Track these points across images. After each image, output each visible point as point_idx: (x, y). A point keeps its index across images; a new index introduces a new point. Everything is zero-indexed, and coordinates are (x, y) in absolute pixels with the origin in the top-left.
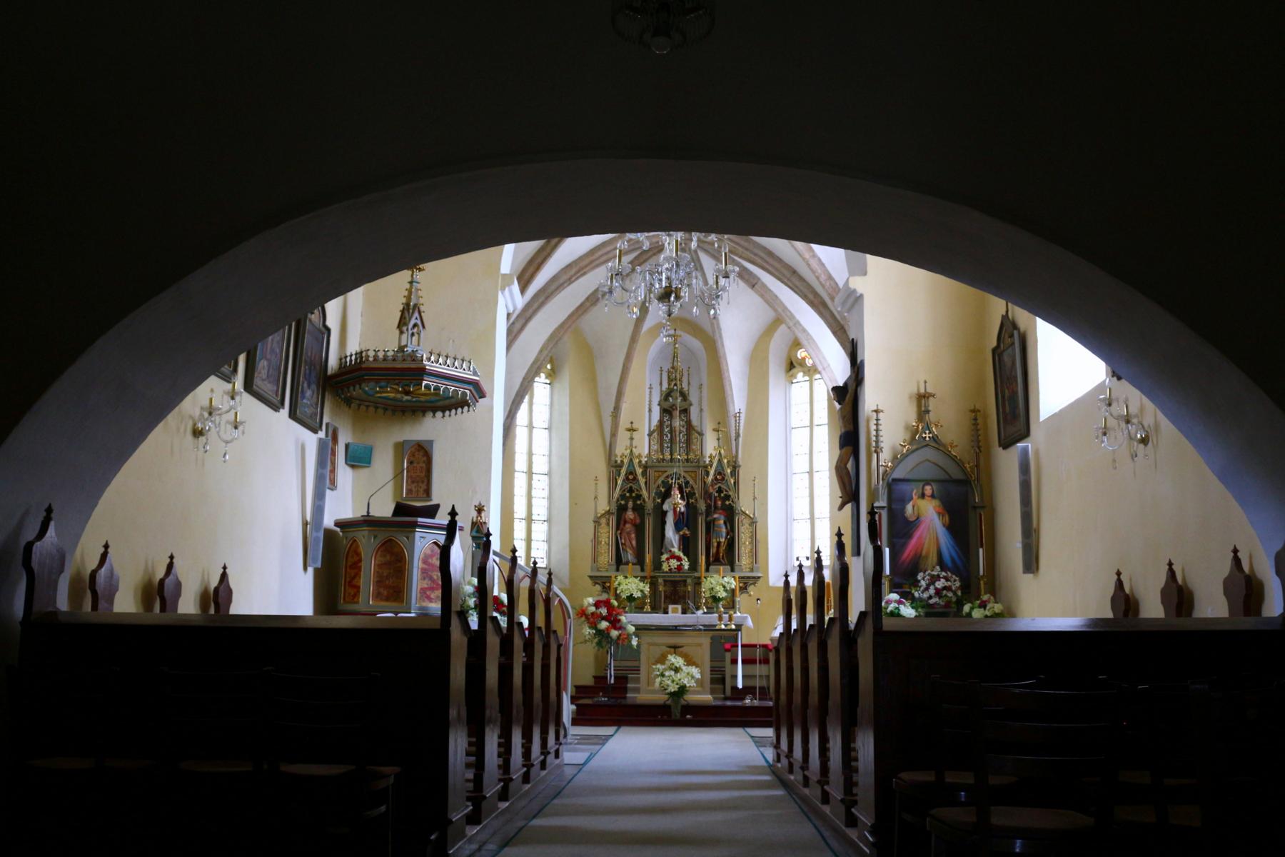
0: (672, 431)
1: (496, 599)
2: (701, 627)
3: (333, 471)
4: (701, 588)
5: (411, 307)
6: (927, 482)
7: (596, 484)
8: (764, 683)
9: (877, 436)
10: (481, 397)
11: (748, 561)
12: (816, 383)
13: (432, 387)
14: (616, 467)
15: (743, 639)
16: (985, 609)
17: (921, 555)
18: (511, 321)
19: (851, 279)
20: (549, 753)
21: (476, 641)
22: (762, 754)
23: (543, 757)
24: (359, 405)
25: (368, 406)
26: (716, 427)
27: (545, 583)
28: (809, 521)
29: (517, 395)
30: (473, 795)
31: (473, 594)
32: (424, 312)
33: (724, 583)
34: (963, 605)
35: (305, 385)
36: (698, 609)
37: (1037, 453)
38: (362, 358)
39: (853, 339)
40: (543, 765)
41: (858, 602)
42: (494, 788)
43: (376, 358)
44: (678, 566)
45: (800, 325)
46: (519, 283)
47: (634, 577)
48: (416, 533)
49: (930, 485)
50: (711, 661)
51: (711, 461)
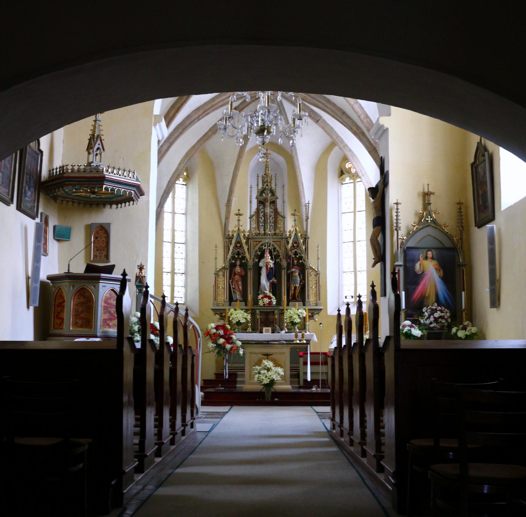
0: (265, 215)
1: (152, 326)
2: (284, 342)
3: (45, 244)
4: (284, 316)
5: (96, 137)
6: (429, 249)
7: (216, 250)
8: (325, 377)
9: (397, 220)
10: (141, 195)
11: (314, 299)
12: (358, 184)
13: (110, 189)
14: (229, 238)
15: (311, 349)
16: (466, 331)
17: (424, 297)
18: (161, 144)
19: (380, 118)
20: (187, 425)
21: (140, 356)
22: (323, 424)
23: (183, 428)
24: (62, 201)
25: (68, 201)
26: (293, 212)
27: (184, 315)
28: (353, 273)
29: (164, 192)
30: (139, 454)
31: (137, 322)
32: (104, 140)
33: (298, 313)
34: (452, 328)
35: (27, 188)
36: (282, 330)
37: (499, 230)
38: (63, 170)
39: (382, 157)
40: (183, 433)
41: (384, 330)
42: (152, 449)
43: (73, 170)
44: (269, 302)
45: (348, 147)
46: (165, 120)
47: (241, 309)
48: (100, 283)
49: (431, 251)
50: (290, 363)
51: (290, 235)
